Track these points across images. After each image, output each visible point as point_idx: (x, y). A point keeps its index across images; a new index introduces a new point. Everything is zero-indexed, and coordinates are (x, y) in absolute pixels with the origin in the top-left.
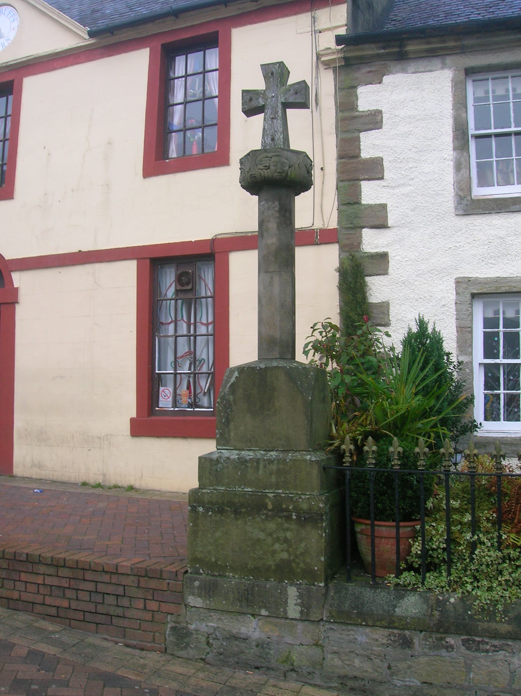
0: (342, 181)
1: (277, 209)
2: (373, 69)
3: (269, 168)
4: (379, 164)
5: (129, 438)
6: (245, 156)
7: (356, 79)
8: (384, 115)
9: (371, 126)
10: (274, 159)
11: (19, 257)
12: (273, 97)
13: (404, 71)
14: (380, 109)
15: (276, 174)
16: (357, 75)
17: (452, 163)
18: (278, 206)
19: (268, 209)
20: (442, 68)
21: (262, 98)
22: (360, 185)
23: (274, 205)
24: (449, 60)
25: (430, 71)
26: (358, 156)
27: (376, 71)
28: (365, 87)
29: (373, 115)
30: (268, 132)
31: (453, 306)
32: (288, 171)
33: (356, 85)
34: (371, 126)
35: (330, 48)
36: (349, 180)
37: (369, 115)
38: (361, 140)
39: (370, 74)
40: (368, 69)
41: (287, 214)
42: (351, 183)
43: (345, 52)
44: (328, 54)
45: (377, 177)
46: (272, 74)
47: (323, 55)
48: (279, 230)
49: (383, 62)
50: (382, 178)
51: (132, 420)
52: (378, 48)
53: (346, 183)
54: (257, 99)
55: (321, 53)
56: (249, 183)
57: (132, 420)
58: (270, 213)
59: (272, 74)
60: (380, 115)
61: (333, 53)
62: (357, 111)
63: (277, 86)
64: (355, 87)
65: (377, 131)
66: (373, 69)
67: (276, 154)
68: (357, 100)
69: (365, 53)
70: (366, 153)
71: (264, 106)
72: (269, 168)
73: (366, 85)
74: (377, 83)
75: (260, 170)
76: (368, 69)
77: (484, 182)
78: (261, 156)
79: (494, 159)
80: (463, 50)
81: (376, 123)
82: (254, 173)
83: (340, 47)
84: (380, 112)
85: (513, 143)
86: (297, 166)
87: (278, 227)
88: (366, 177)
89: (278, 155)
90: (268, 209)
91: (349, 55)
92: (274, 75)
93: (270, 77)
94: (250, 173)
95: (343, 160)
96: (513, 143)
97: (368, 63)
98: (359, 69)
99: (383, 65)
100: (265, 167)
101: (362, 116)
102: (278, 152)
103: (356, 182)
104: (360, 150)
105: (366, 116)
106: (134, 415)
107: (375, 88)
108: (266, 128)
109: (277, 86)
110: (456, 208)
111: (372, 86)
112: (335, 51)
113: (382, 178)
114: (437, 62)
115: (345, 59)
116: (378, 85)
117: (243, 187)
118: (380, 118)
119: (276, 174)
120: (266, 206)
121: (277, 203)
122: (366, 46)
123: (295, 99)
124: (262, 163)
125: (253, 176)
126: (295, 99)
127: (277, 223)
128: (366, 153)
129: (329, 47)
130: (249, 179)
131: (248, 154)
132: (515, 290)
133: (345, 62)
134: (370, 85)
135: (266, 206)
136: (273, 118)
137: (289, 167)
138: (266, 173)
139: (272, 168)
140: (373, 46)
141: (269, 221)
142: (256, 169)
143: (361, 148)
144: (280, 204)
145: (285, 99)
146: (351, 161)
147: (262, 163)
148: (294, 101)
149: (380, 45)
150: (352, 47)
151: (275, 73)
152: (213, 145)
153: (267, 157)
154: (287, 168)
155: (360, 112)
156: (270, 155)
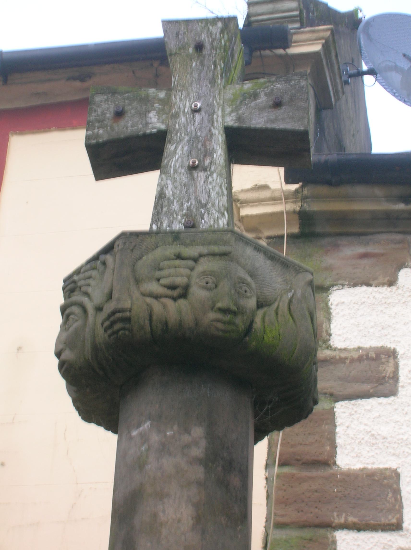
0: (279, 526)
1: (198, 452)
2: (370, 249)
3: (184, 295)
4: (390, 486)
6: (89, 262)
7: (329, 269)
8: (402, 363)
9: (366, 387)
10: (204, 265)
12: (196, 111)
14: (391, 346)
15: (212, 315)
16: (330, 260)
18: (203, 443)
19: (164, 449)
21: (159, 112)
22: (334, 542)
23: (186, 438)
26: (327, 462)
27: (382, 255)
28: (352, 290)
29: (372, 359)
30: (176, 206)
32: (253, 314)
33: (328, 283)
34: (366, 387)
35: (265, 187)
36: (303, 526)
37: (360, 359)
38: (338, 421)
39: (365, 262)
40: (361, 250)
41: (235, 480)
42: (307, 533)
43: (304, 199)
44: (259, 202)
45: (383, 520)
46: (199, 47)
48: (204, 532)
49: (399, 237)
50: (397, 527)
52: (389, 199)
53: (294, 534)
54: (143, 114)
55: (242, 197)
56: (95, 348)
58: (168, 463)
59: (199, 47)
60: (391, 360)
61: (274, 200)
62: (329, 347)
63: (213, 82)
64: (325, 289)
65: (382, 400)
66: (370, 249)
67: (216, 249)
68: (329, 320)
69: (357, 206)
70: (350, 457)
71: (161, 137)
72: (184, 295)
73: (354, 285)
74: (383, 284)
75: (149, 300)
76: (361, 250)
78: (159, 253)
81: (381, 380)
82: (127, 304)
83: (294, 187)
84: (392, 354)
86: (284, 307)
87: (198, 519)
88: (351, 519)
89: (224, 255)
90: (164, 449)
91: (315, 207)
92: (206, 51)
93: (190, 58)
94: (109, 308)
95: (286, 470)
97: (359, 235)
98: (336, 246)
99: (399, 242)
100: (173, 287)
101: (342, 360)
102: (226, 243)
103: (322, 531)
104: (334, 446)
105: (353, 361)
107: (377, 296)
108: (169, 192)
109: (213, 82)
111: (370, 289)
112: (277, 194)
113: (397, 527)
115: (305, 218)
116: (385, 290)
117: (67, 370)
118: (390, 369)
119: (212, 315)
120: (155, 438)
121: (198, 432)
122: (360, 190)
123: (272, 121)
124: (158, 274)
125: (119, 320)
126: (272, 121)
127: (196, 506)
128: (350, 457)
129: (262, 183)
130: (100, 331)
131: (109, 249)
133: (302, 226)
134: (364, 288)
135: (155, 438)
136: (193, 168)
137: (260, 306)
138: (173, 311)
139: (198, 293)
140: (378, 191)
141: (161, 496)
142: (136, 294)
143: (339, 441)
144: (211, 436)
145: (239, 119)
146: (306, 473)
147: (158, 274)
148: (270, 126)
149: (396, 190)
150: (323, 190)
151: (208, 46)
153: (179, 257)
154: (252, 303)
155: (335, 349)
156: (193, 251)
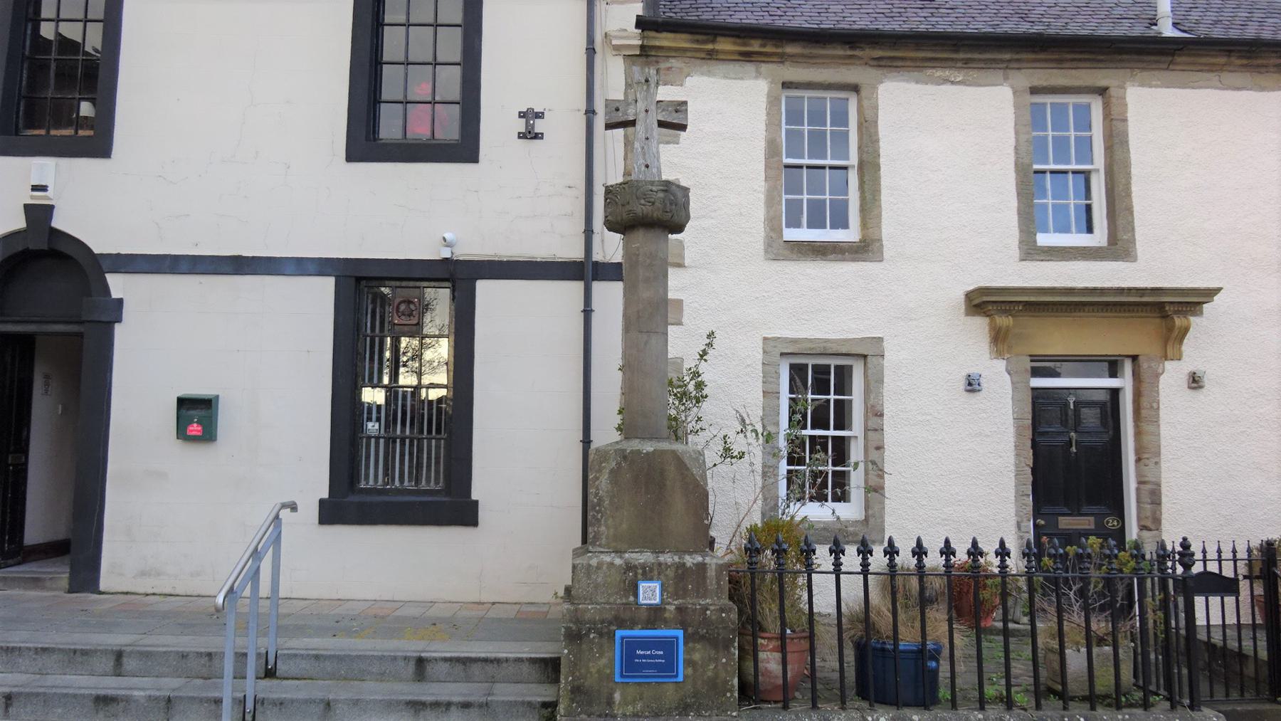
5: (962, 317)
11: (245, 254)
13: (709, 74)
17: (762, 197)
20: (756, 78)
24: (764, 68)
25: (742, 79)
31: (760, 367)
47: (616, 37)
51: (322, 502)
57: (322, 502)
77: (794, 223)
79: (805, 197)
80: (782, 58)
85: (1049, 186)
96: (1049, 186)
106: (325, 495)
110: (766, 252)
114: (750, 68)
132: (830, 351)
152: (449, 130)
